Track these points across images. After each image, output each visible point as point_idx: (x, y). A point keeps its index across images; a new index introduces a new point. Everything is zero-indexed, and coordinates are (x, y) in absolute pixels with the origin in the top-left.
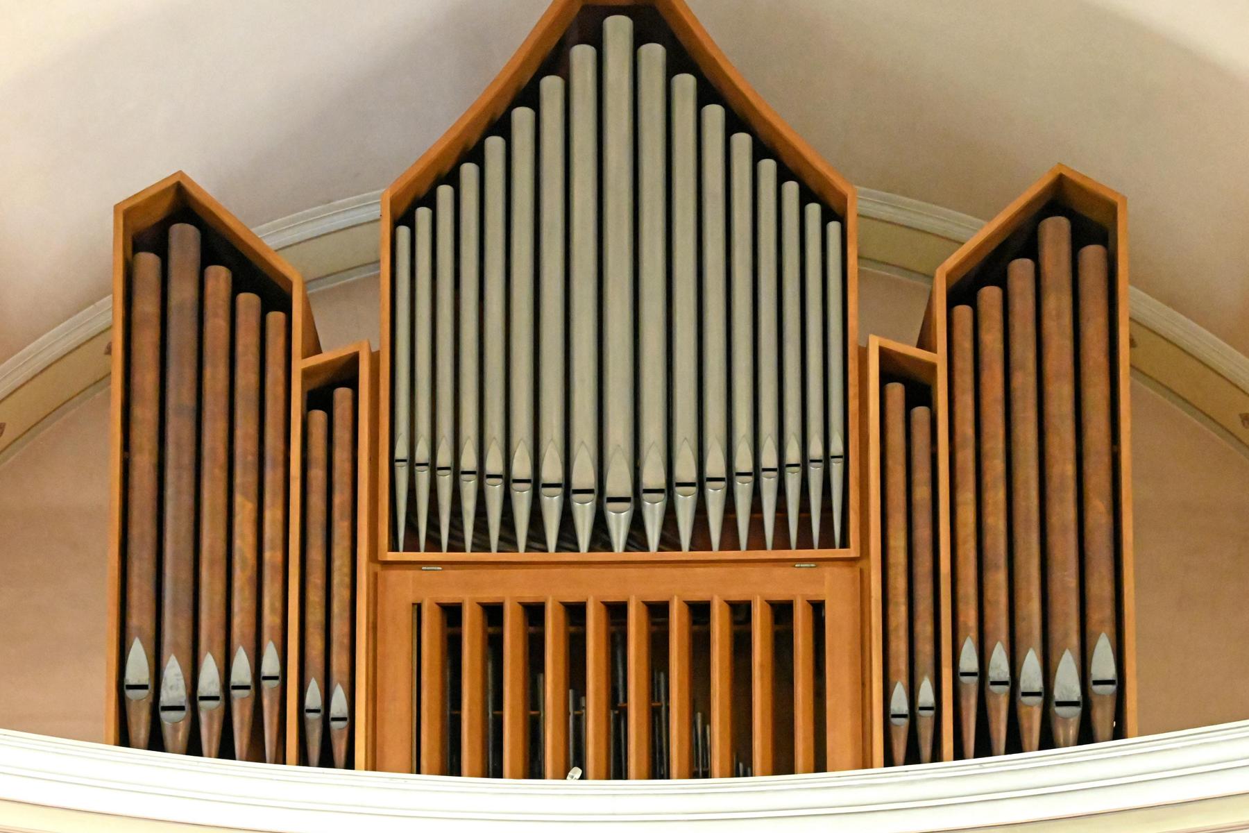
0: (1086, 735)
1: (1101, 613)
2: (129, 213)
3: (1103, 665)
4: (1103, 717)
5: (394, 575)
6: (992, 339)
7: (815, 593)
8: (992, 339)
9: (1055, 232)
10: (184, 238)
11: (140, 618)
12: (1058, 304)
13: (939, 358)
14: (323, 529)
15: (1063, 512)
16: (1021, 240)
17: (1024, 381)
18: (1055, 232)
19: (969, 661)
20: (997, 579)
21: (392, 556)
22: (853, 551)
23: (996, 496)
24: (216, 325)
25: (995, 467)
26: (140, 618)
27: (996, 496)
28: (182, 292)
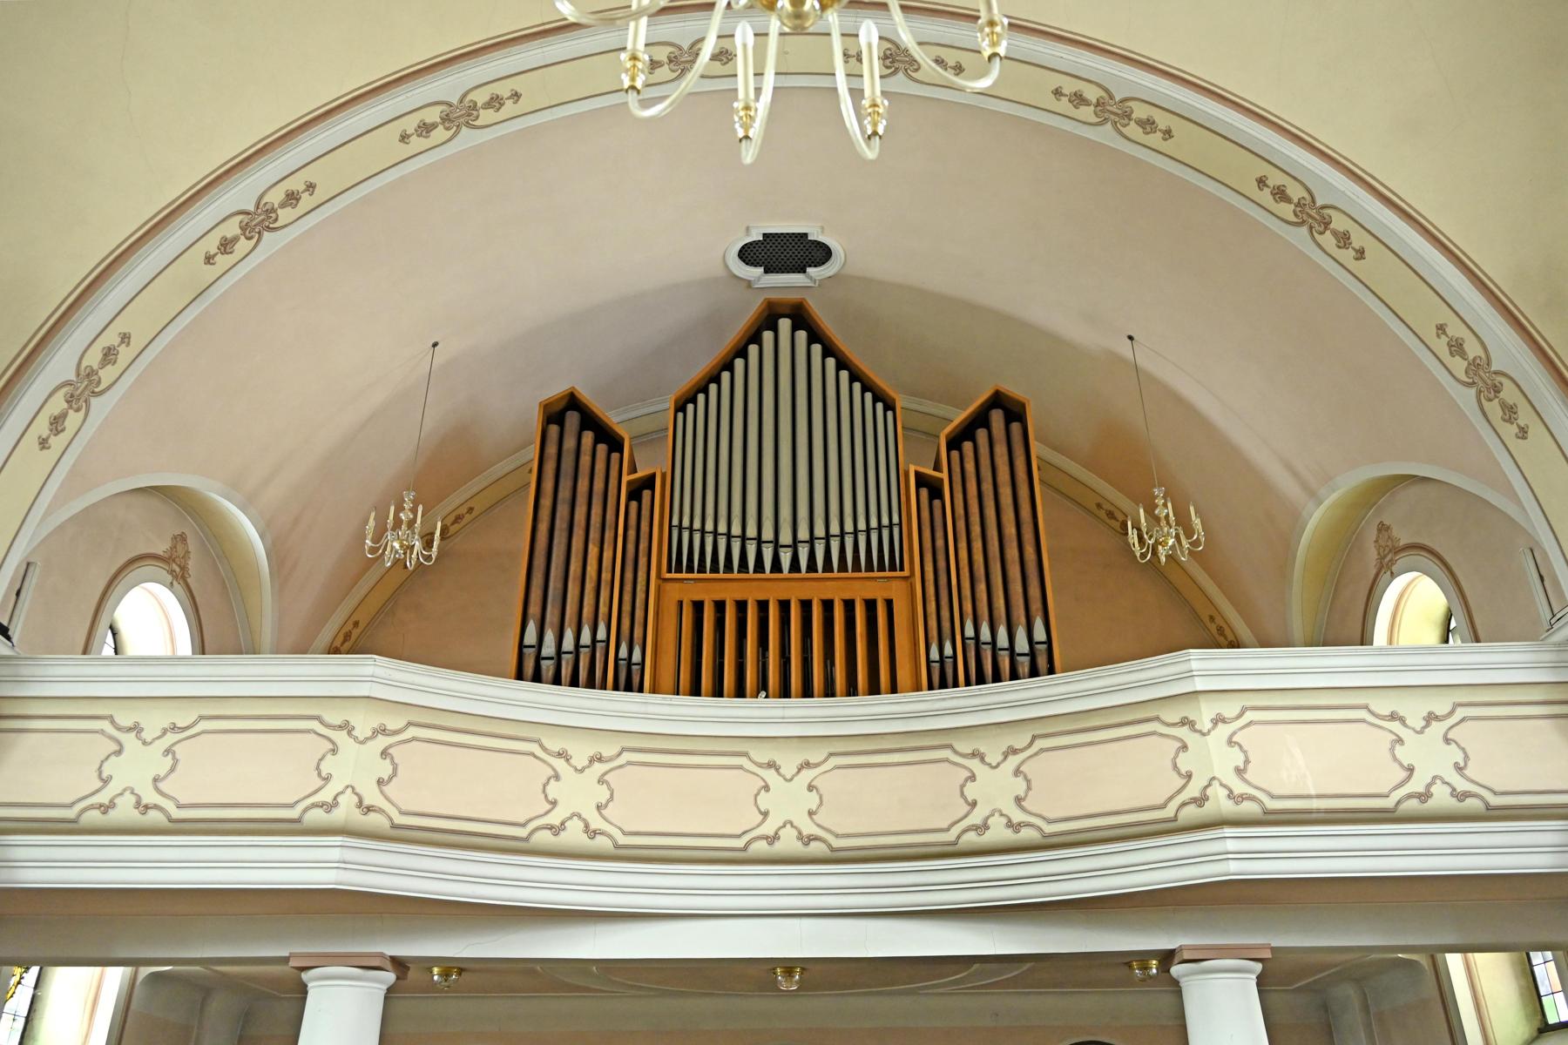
0: (1034, 672)
1: (1036, 605)
2: (546, 406)
3: (1040, 634)
4: (1042, 662)
5: (668, 586)
6: (970, 467)
7: (887, 595)
8: (970, 467)
9: (997, 417)
10: (572, 419)
11: (534, 609)
12: (1001, 450)
13: (945, 475)
14: (633, 563)
15: (1012, 553)
16: (980, 420)
17: (987, 487)
18: (997, 417)
19: (970, 632)
20: (981, 587)
21: (668, 576)
22: (906, 573)
23: (977, 545)
24: (585, 460)
25: (976, 529)
26: (534, 609)
27: (977, 545)
28: (569, 443)
